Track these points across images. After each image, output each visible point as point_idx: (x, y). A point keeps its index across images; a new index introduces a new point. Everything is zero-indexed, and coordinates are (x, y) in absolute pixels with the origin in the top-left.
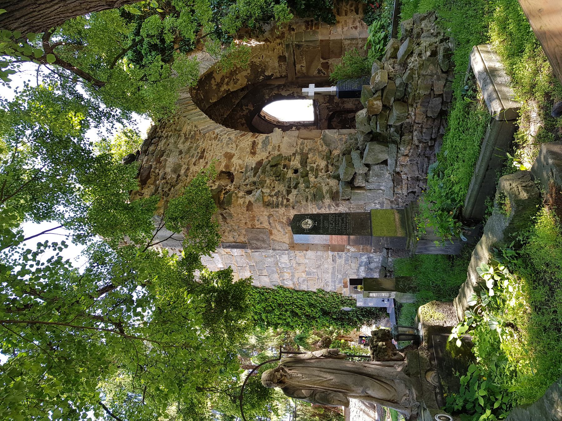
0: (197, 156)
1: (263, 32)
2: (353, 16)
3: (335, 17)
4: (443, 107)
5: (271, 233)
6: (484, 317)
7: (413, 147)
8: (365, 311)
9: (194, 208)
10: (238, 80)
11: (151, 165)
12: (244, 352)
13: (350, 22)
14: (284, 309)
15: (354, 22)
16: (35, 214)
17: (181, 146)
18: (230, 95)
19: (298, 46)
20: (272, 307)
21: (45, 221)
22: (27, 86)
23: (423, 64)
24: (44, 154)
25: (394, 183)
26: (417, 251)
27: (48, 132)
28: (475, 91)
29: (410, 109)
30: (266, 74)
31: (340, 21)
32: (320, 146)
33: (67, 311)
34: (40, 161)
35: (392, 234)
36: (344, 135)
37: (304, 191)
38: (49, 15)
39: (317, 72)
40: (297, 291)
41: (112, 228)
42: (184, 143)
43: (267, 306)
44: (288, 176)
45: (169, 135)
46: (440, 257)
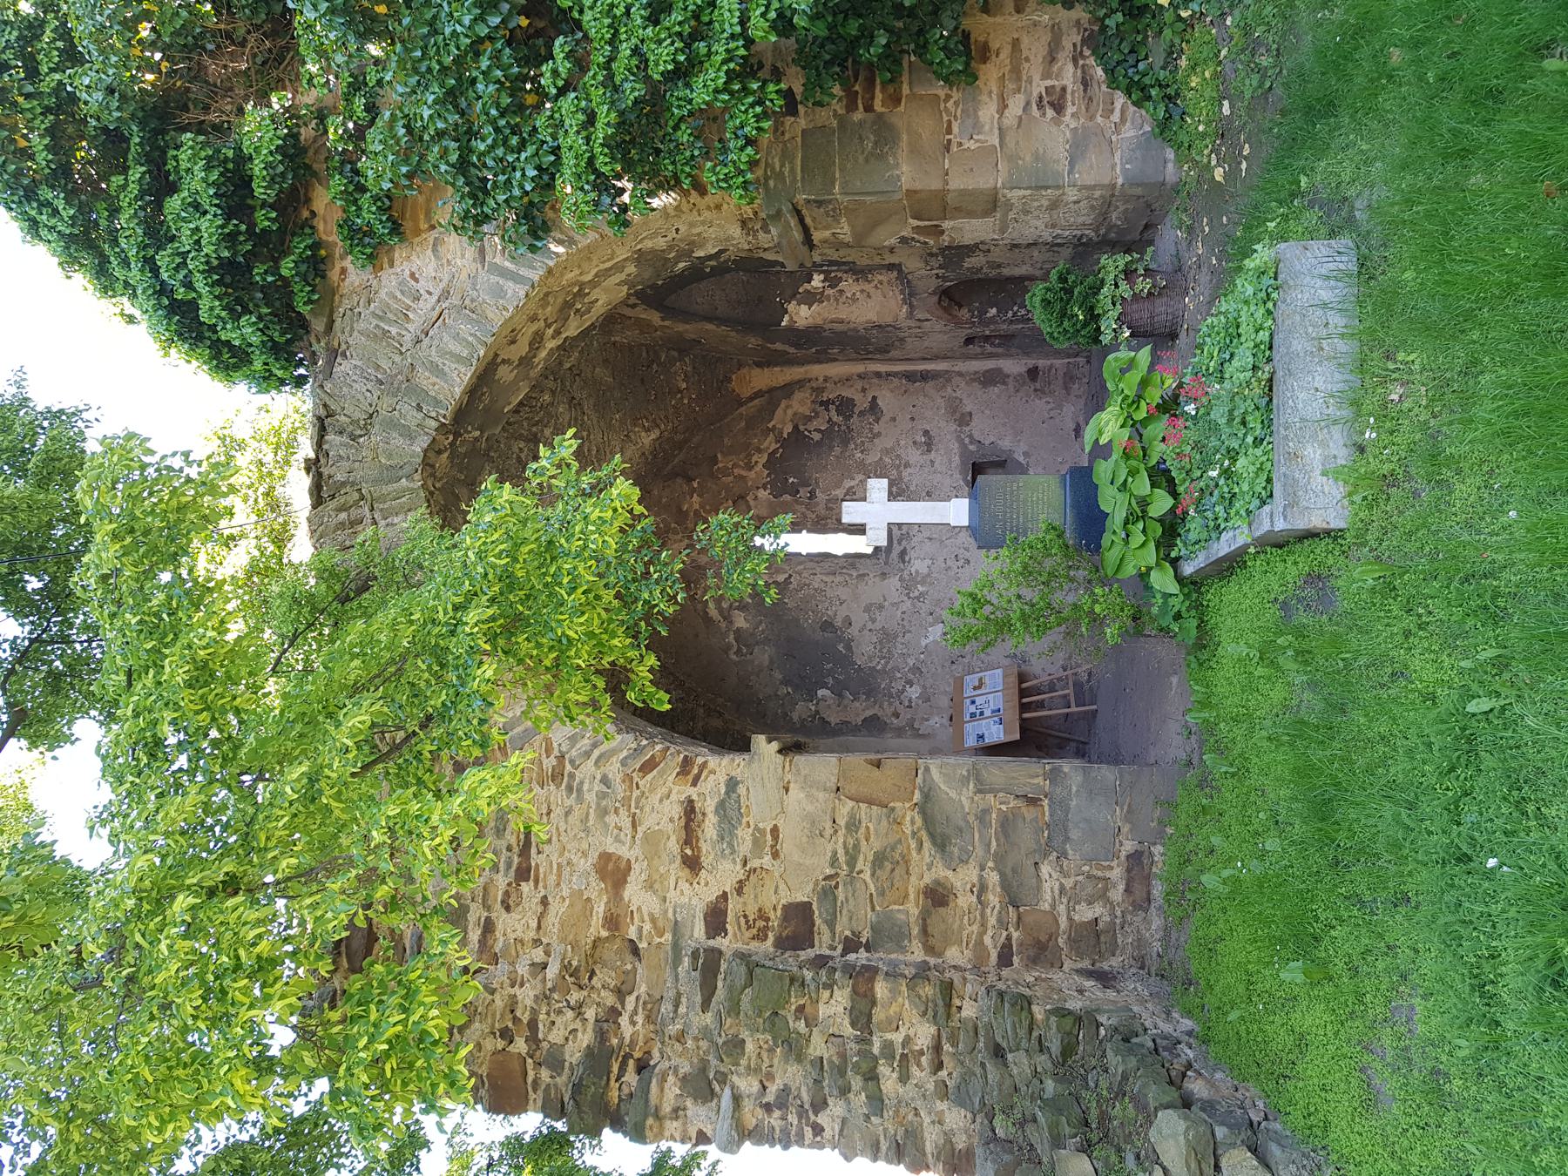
0: (509, 865)
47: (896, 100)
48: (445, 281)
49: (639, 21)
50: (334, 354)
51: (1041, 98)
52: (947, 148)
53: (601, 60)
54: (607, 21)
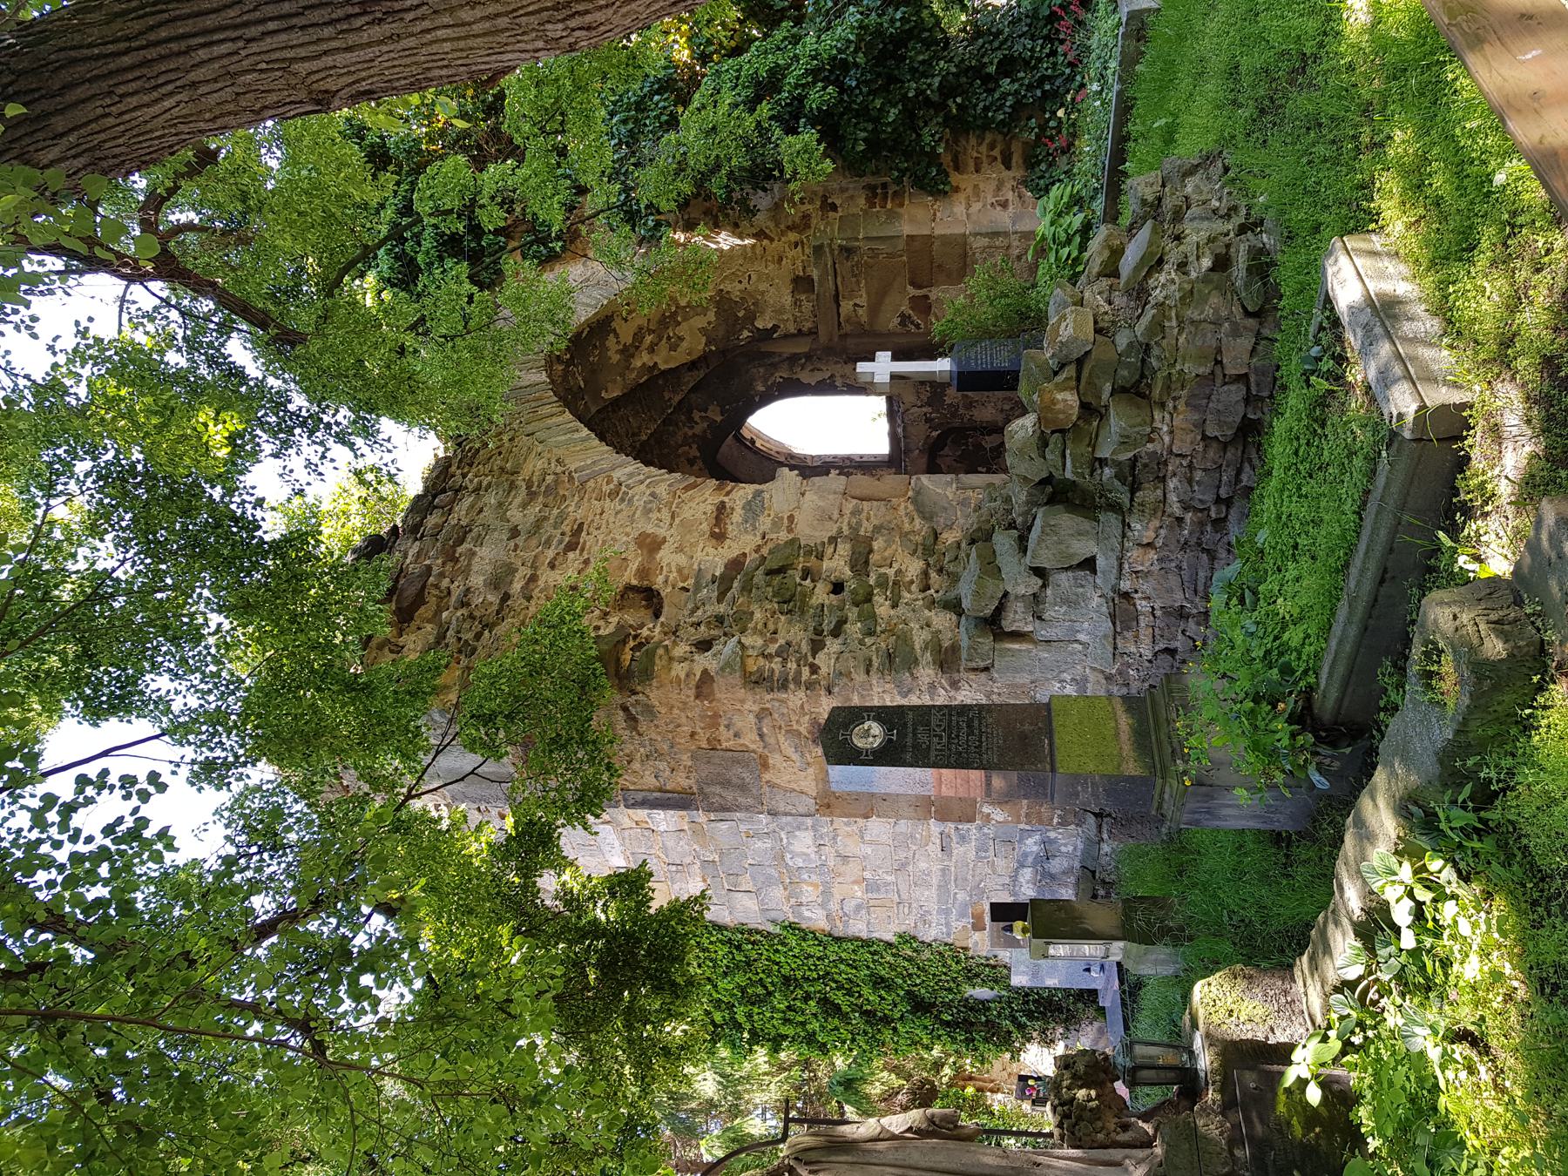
0: (560, 542)
1: (752, 212)
2: (995, 173)
3: (947, 175)
4: (1250, 409)
5: (765, 765)
6: (1386, 1014)
7: (1167, 521)
8: (1035, 1001)
9: (547, 689)
10: (681, 339)
11: (429, 568)
12: (682, 1121)
13: (988, 189)
14: (799, 993)
15: (999, 189)
16: (86, 699)
17: (515, 515)
18: (658, 380)
19: (848, 251)
20: (765, 988)
21: (114, 720)
22: (83, 334)
23: (1191, 292)
24: (124, 530)
25: (1114, 624)
26: (1186, 817)
27: (140, 467)
28: (1341, 359)
29: (1157, 415)
30: (759, 324)
31: (962, 186)
32: (906, 520)
33: (153, 983)
34: (112, 550)
35: (1109, 769)
36: (973, 489)
37: (861, 642)
38: (149, 126)
39: (897, 321)
40: (838, 939)
41: (308, 743)
42: (524, 506)
43: (752, 983)
44: (814, 601)
45: (485, 483)
46: (1249, 838)
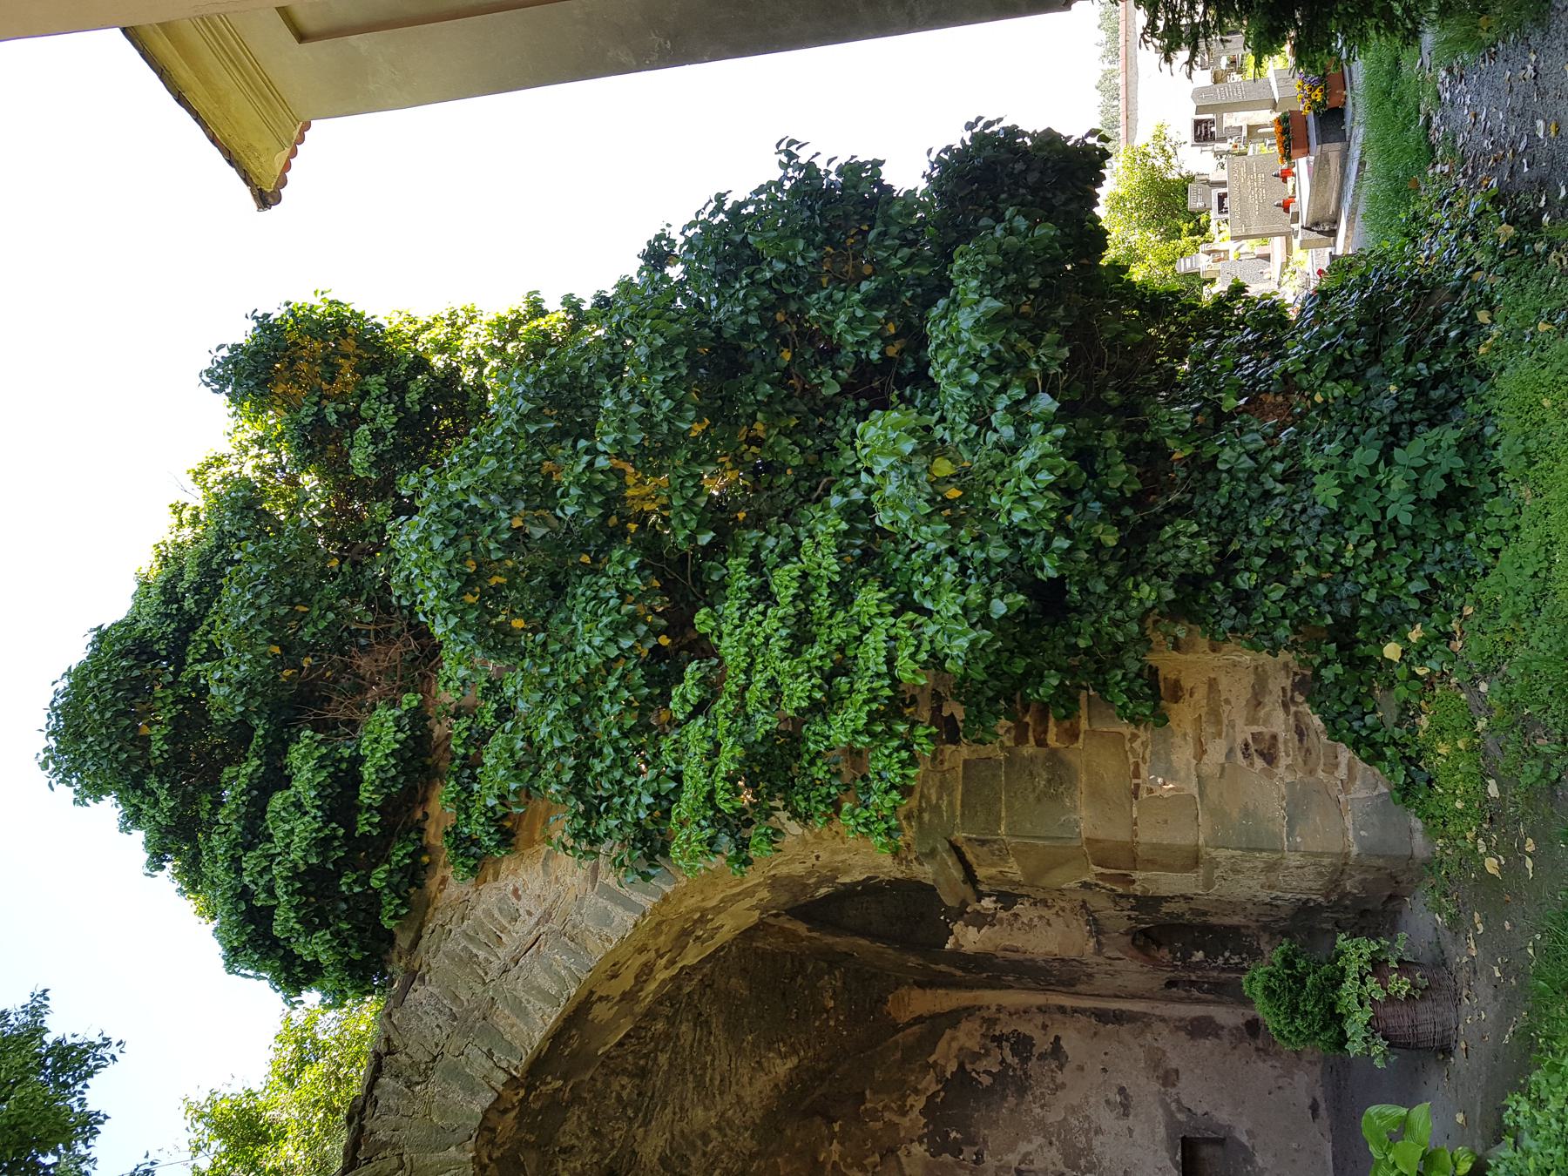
47: (1073, 735)
48: (549, 902)
49: (777, 652)
50: (412, 976)
51: (1247, 745)
52: (1135, 793)
53: (734, 689)
54: (744, 650)
